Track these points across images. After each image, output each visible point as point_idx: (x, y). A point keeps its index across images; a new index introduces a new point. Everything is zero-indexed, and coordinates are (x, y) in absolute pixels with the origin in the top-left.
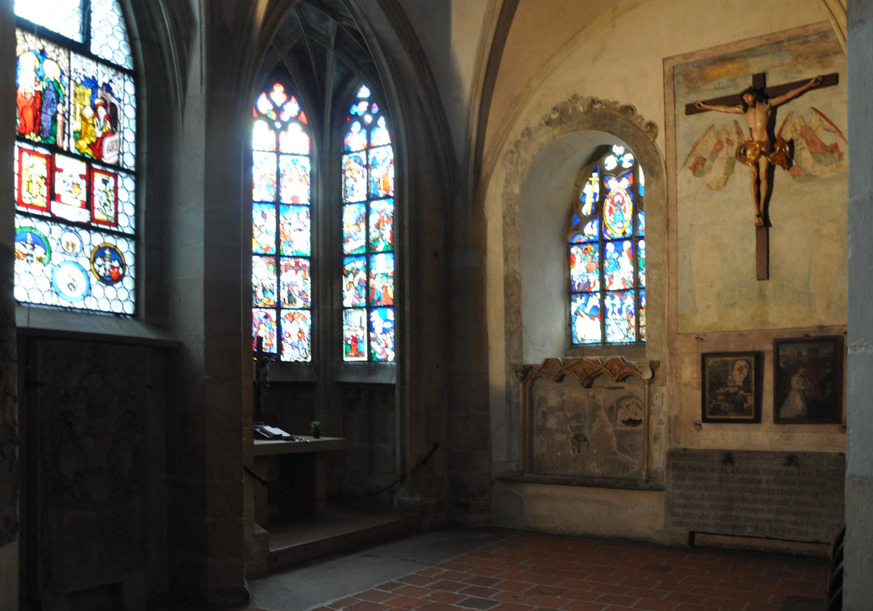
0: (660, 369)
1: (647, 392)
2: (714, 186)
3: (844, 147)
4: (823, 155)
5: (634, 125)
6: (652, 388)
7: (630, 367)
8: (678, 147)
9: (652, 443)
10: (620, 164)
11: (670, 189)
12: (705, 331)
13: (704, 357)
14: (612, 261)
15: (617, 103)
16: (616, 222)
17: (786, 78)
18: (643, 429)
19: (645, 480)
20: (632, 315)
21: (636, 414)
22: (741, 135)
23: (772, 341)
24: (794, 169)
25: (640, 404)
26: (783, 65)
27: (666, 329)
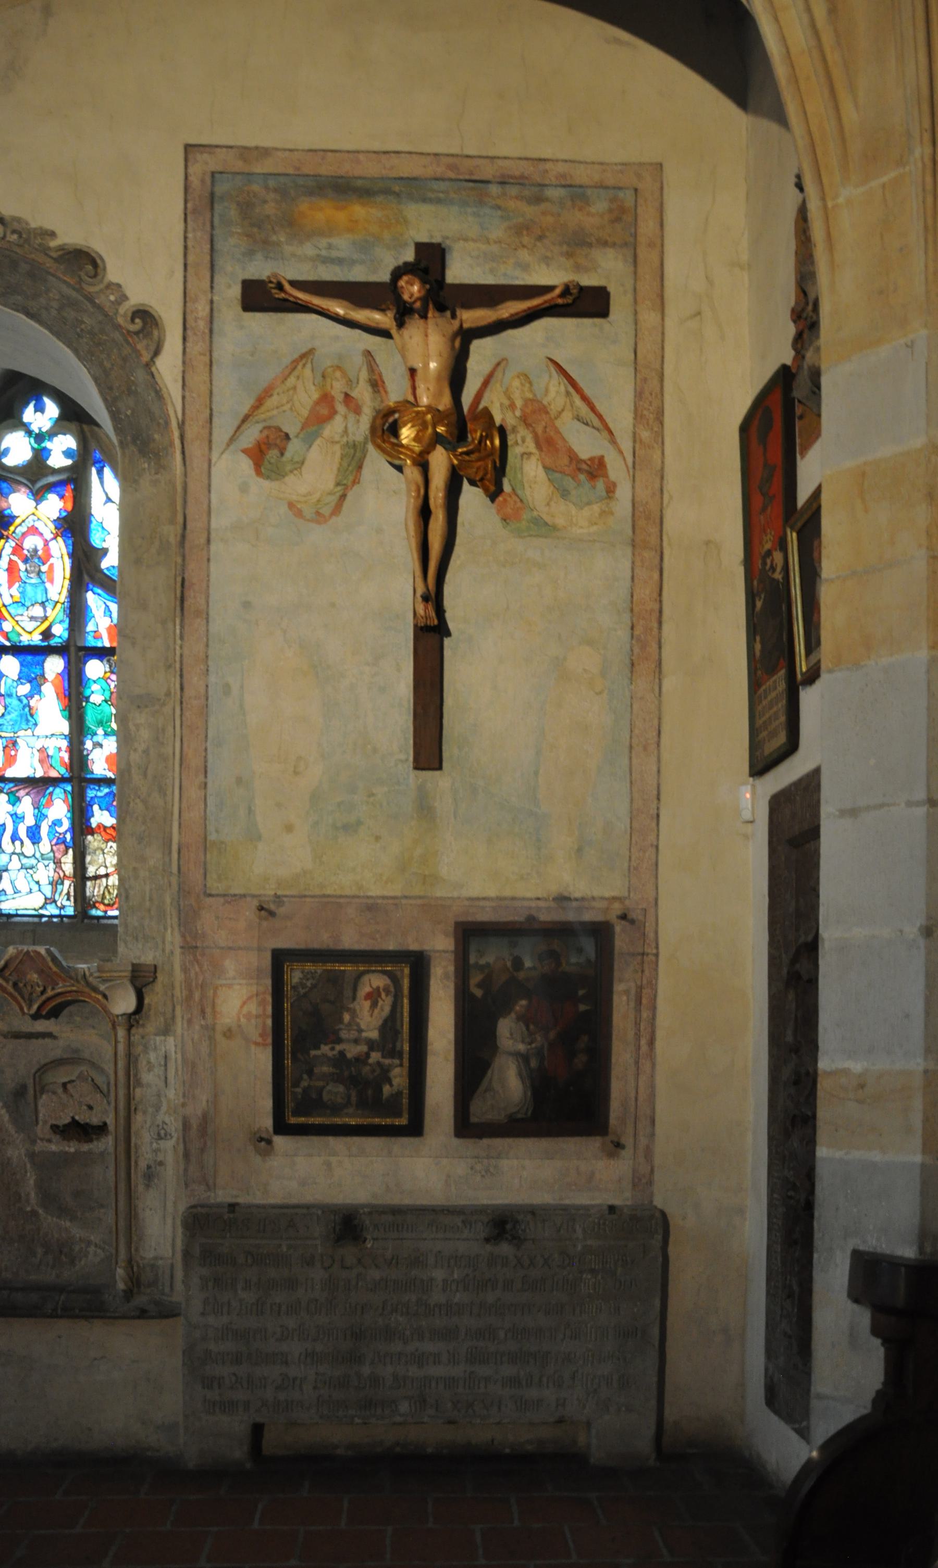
0: (158, 987)
1: (121, 1048)
2: (308, 512)
3: (616, 469)
4: (573, 478)
5: (99, 308)
6: (135, 1038)
7: (71, 978)
8: (215, 391)
9: (141, 1188)
10: (40, 456)
11: (190, 500)
12: (279, 893)
13: (280, 959)
14: (14, 702)
15: (53, 234)
16: (28, 604)
17: (492, 271)
18: (111, 1149)
19: (124, 1291)
20: (67, 848)
21: (90, 1108)
22: (382, 391)
23: (451, 929)
24: (505, 500)
25: (100, 1080)
26: (488, 241)
27: (174, 880)
